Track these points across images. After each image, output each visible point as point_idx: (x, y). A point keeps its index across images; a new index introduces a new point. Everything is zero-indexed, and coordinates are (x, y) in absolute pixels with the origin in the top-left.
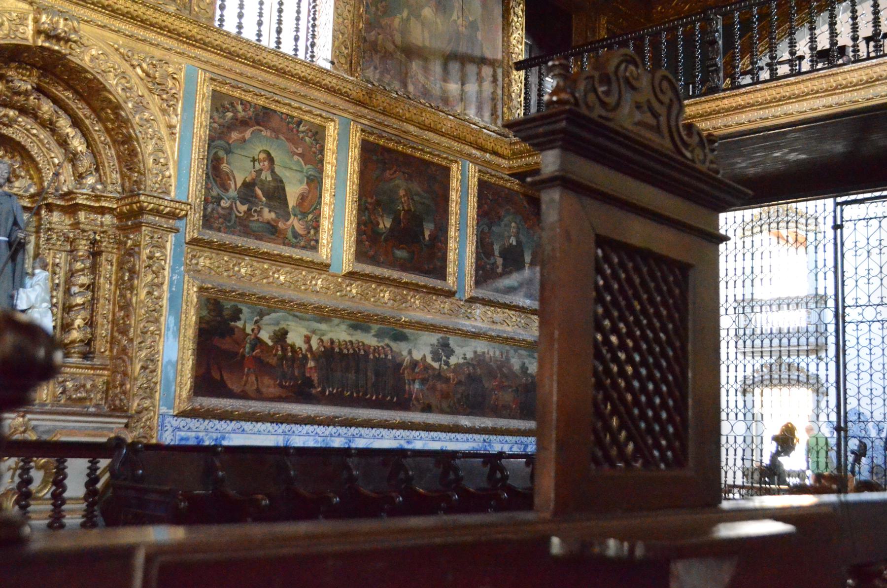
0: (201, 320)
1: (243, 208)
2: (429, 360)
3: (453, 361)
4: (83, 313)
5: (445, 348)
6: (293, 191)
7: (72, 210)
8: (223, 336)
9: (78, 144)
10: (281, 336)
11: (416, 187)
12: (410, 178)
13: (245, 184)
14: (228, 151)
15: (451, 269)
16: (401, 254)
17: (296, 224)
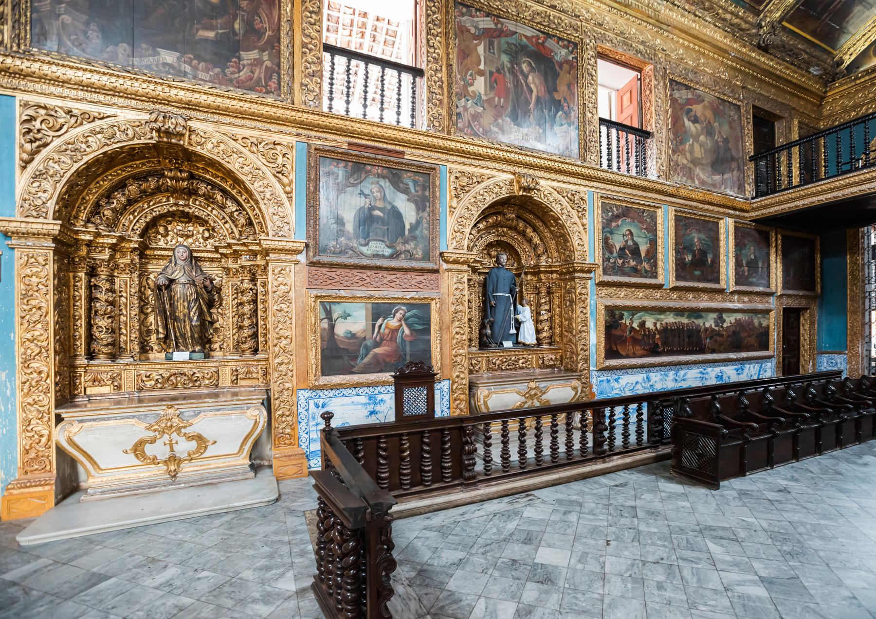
0: (606, 321)
1: (620, 262)
2: (713, 326)
3: (725, 325)
4: (548, 324)
5: (721, 320)
6: (643, 249)
7: (536, 273)
8: (616, 328)
9: (536, 240)
10: (642, 324)
11: (702, 236)
12: (699, 231)
13: (620, 249)
14: (611, 233)
15: (723, 277)
16: (697, 273)
17: (645, 265)
